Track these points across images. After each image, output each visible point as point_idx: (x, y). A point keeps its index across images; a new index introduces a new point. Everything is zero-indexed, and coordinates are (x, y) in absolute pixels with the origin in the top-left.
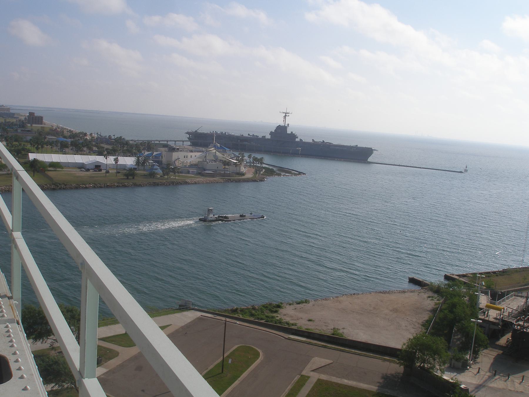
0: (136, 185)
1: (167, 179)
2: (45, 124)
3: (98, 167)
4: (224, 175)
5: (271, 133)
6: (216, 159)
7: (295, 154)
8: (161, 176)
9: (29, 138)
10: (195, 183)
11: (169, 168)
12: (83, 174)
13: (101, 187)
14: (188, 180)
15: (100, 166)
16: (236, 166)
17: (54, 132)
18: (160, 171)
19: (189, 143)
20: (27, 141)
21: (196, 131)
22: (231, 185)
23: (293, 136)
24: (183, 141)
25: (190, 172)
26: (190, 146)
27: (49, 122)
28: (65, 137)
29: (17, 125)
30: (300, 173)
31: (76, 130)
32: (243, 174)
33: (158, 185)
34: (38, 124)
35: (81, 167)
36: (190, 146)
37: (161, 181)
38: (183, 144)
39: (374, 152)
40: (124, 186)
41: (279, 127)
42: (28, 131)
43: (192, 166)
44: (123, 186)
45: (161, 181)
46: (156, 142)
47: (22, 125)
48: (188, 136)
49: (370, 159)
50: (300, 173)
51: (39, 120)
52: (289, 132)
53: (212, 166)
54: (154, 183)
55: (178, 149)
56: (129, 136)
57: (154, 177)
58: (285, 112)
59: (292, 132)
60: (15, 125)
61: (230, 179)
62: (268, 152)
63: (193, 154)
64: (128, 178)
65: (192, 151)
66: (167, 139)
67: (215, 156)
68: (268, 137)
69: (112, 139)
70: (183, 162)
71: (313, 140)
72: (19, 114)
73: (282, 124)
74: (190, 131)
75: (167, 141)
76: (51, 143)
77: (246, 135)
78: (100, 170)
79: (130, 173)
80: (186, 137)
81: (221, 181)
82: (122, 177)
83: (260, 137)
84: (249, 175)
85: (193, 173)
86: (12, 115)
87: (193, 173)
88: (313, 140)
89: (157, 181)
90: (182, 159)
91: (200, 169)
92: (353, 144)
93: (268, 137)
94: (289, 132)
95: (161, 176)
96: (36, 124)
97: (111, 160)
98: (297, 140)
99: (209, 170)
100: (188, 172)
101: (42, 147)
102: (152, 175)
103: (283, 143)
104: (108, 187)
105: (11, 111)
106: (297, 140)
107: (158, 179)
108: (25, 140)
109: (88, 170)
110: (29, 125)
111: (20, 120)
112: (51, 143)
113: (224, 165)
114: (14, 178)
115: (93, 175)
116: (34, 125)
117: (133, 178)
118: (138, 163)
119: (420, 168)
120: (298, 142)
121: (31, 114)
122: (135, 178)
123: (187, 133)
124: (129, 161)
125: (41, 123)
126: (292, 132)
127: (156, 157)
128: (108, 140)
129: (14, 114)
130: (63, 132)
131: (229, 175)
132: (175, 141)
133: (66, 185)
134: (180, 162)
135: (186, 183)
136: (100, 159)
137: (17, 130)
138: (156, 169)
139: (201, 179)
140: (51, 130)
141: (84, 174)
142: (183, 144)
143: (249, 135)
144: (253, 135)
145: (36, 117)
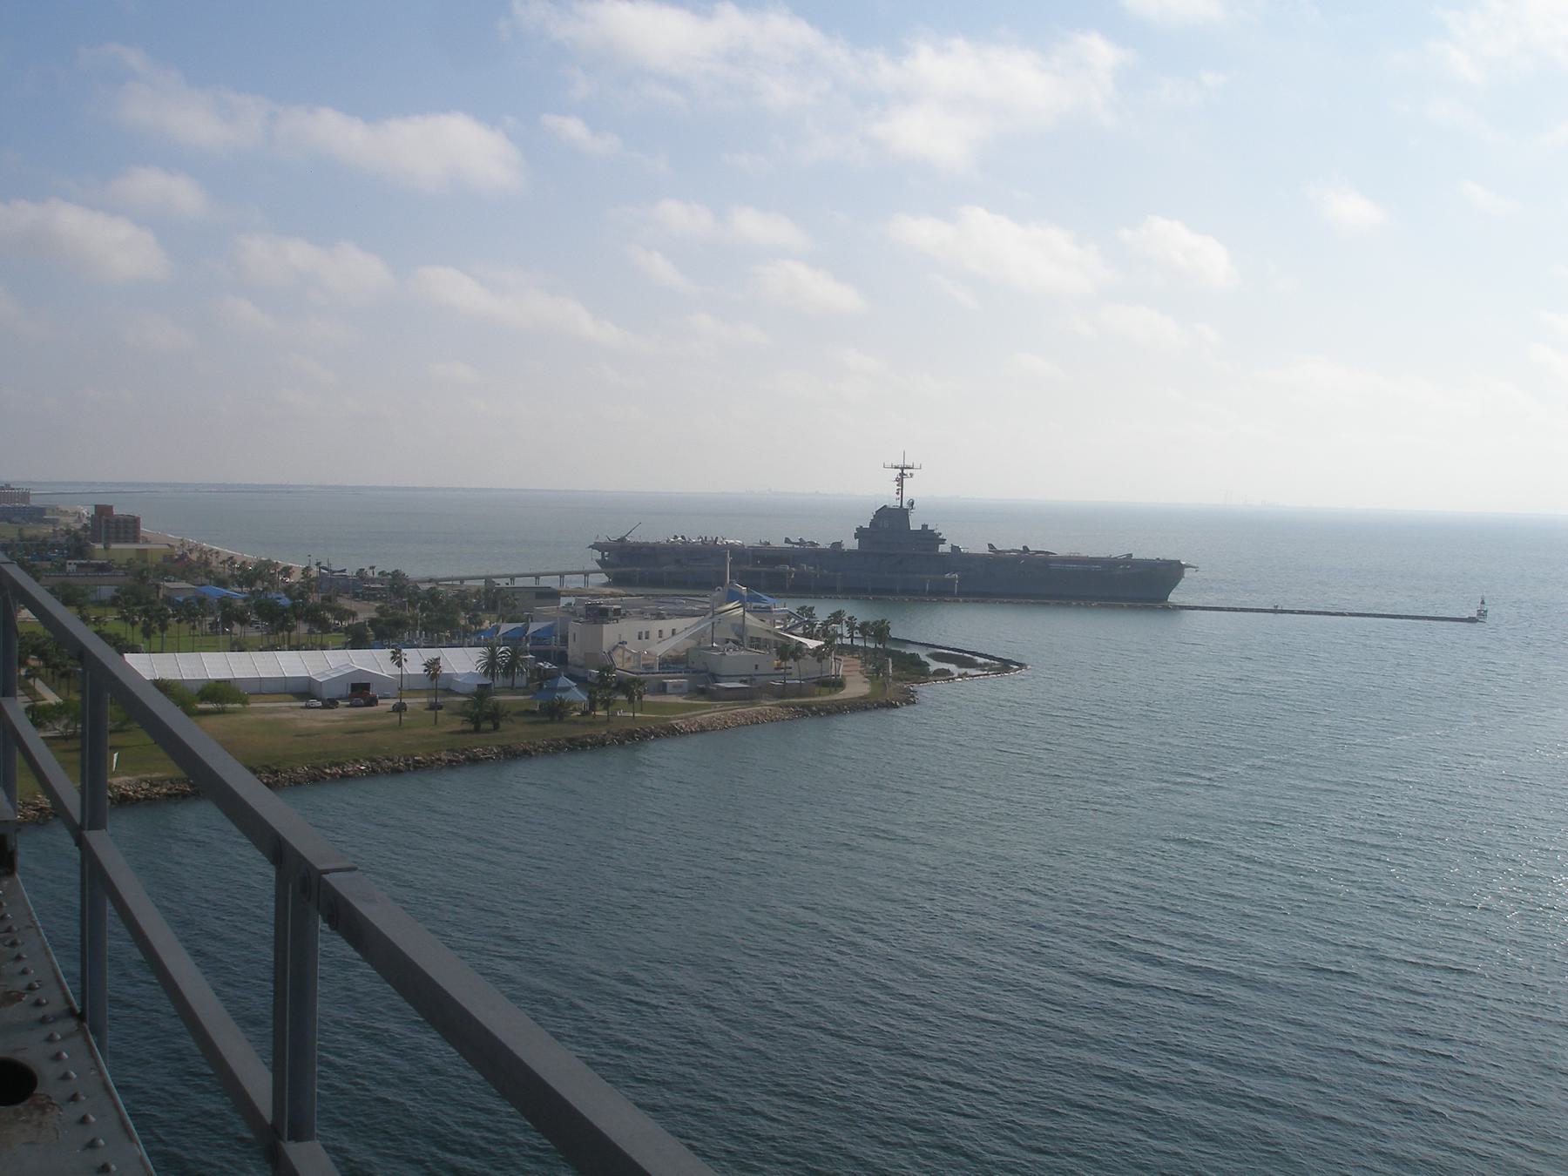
0: (511, 754)
1: (608, 720)
2: (147, 541)
3: (361, 691)
4: (782, 693)
5: (860, 533)
6: (741, 638)
7: (942, 594)
8: (584, 713)
9: (107, 592)
10: (702, 730)
11: (608, 685)
12: (318, 719)
13: (396, 771)
14: (677, 721)
15: (366, 686)
16: (819, 661)
17: (181, 564)
18: (578, 696)
19: (605, 579)
20: (101, 604)
21: (622, 540)
22: (809, 730)
23: (929, 538)
24: (586, 574)
25: (669, 689)
26: (606, 585)
27: (161, 532)
28: (222, 583)
29: (59, 546)
30: (1005, 666)
31: (249, 555)
32: (839, 684)
33: (583, 745)
34: (126, 541)
35: (304, 691)
36: (606, 585)
37: (590, 731)
38: (586, 583)
39: (1188, 573)
40: (474, 761)
41: (884, 514)
42: (102, 568)
43: (671, 663)
44: (468, 759)
45: (590, 731)
46: (519, 583)
47: (76, 545)
48: (598, 555)
49: (1174, 598)
50: (1005, 666)
51: (128, 528)
52: (915, 526)
53: (738, 659)
54: (571, 740)
55: (617, 612)
56: (422, 567)
57: (561, 717)
58: (900, 464)
59: (925, 526)
60: (53, 547)
61: (807, 706)
62: (854, 591)
63: (666, 625)
64: (477, 730)
65: (659, 616)
66: (534, 571)
67: (741, 629)
68: (851, 544)
69: (373, 581)
70: (638, 655)
71: (991, 546)
72: (55, 510)
73: (893, 502)
74: (603, 540)
75: (537, 576)
76: (189, 611)
77: (778, 542)
78: (372, 702)
79: (480, 710)
80: (591, 559)
81: (782, 713)
82: (456, 726)
83: (824, 544)
84: (857, 687)
85: (678, 689)
86: (37, 515)
87: (678, 689)
88: (991, 546)
89: (579, 733)
90: (633, 647)
91: (698, 675)
92: (1116, 551)
93: (851, 544)
94: (915, 526)
95: (584, 713)
96: (118, 541)
97: (415, 661)
98: (944, 548)
99: (730, 677)
100: (662, 689)
101: (164, 627)
102: (555, 711)
103: (897, 559)
104: (418, 766)
105: (34, 502)
106: (944, 548)
107: (575, 722)
108: (92, 597)
109: (331, 704)
110: (99, 546)
111: (68, 532)
112: (189, 611)
113: (784, 658)
114: (326, 877)
115: (358, 724)
116: (114, 546)
117: (496, 727)
118: (491, 665)
119: (1343, 614)
120: (943, 555)
121: (103, 511)
122: (502, 725)
123: (596, 546)
124: (462, 663)
125: (136, 539)
126: (925, 526)
127: (537, 638)
128: (359, 586)
129: (42, 511)
130: (207, 563)
131: (799, 692)
132: (562, 575)
133: (275, 773)
134: (627, 655)
135: (672, 732)
136: (373, 662)
137: (64, 565)
138: (567, 689)
139: (713, 713)
140: (168, 558)
141: (318, 719)
142: (586, 583)
143: (787, 541)
144: (801, 542)
145: (118, 521)
